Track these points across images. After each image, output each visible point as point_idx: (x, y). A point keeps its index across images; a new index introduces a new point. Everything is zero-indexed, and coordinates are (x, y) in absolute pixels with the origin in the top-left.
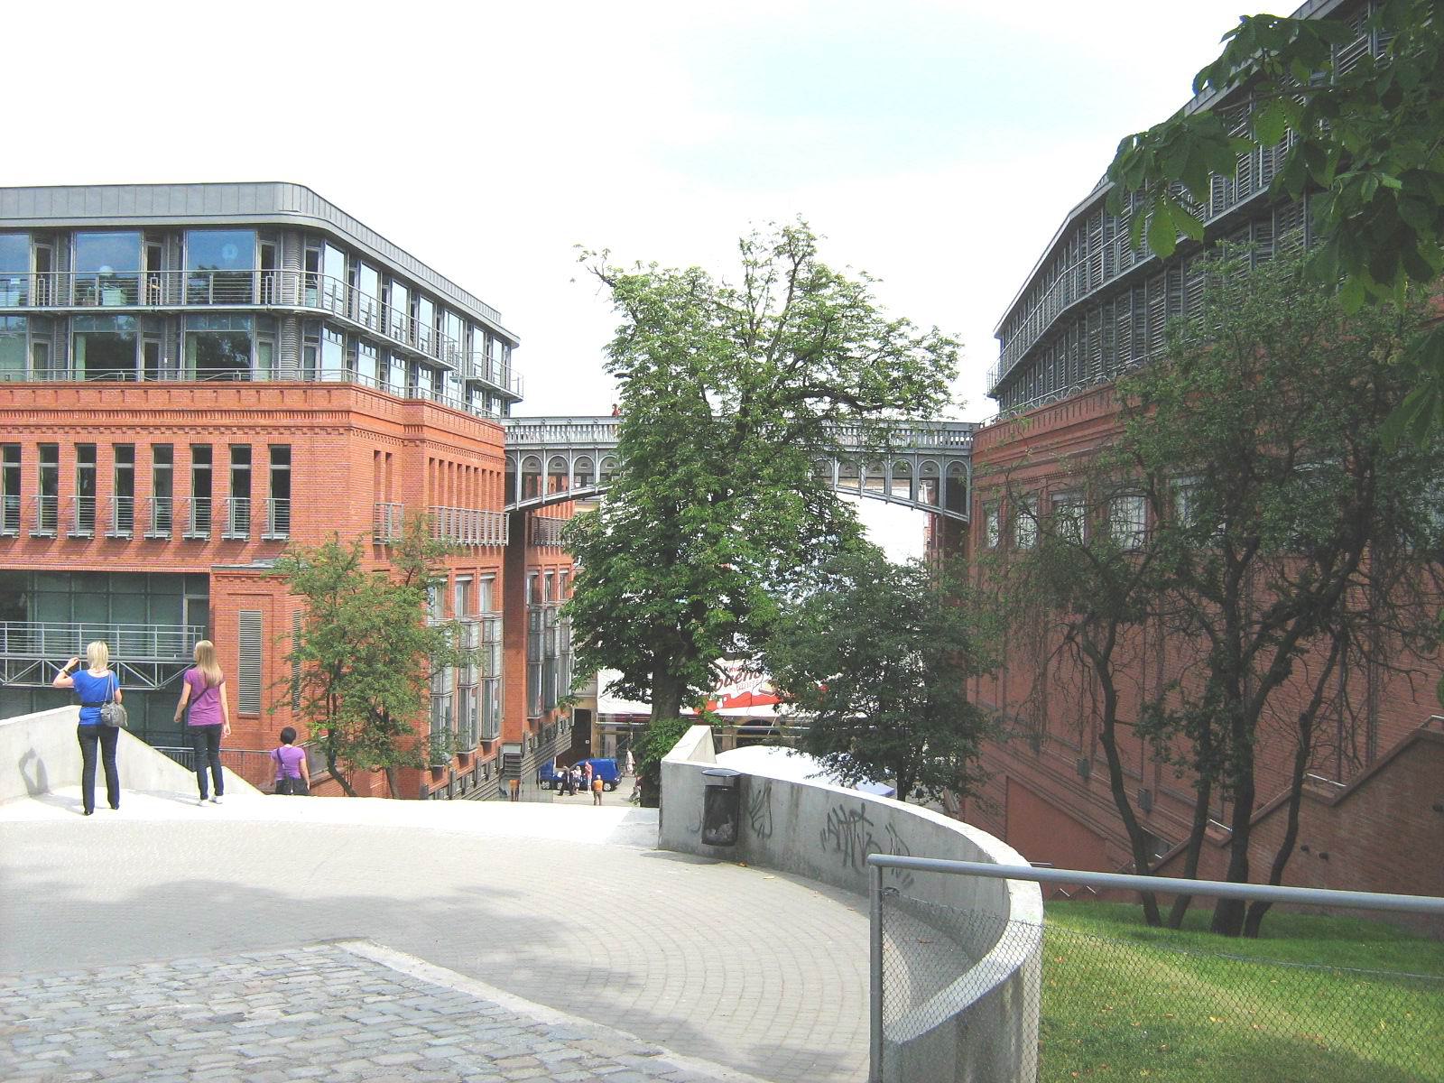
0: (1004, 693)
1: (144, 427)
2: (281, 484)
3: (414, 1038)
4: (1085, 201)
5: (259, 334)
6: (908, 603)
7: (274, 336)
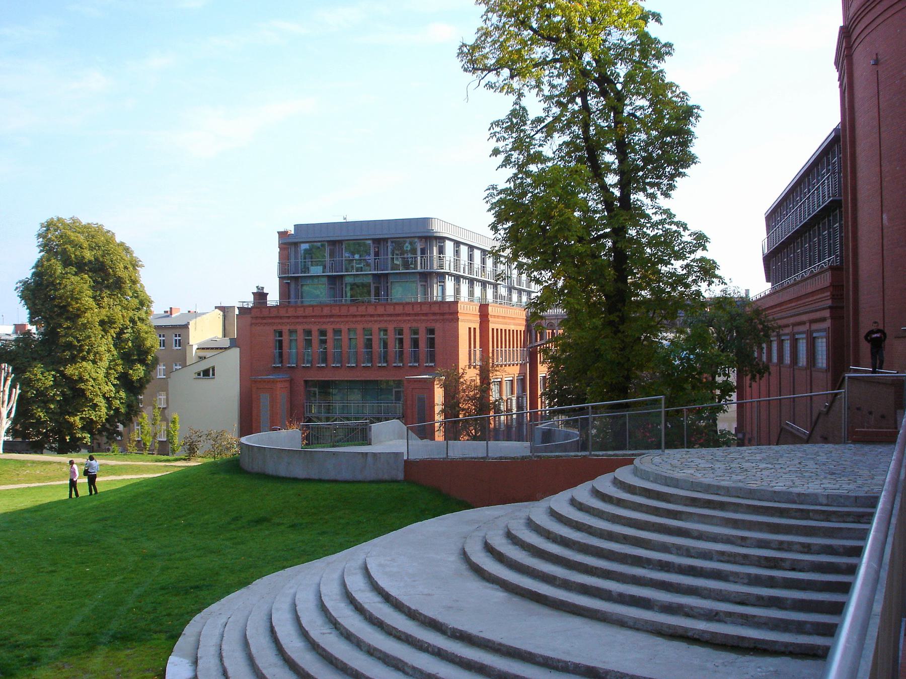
0: (864, 16)
1: (376, 321)
2: (432, 343)
3: (864, 468)
4: (820, 147)
5: (420, 281)
6: (671, 242)
7: (426, 282)
